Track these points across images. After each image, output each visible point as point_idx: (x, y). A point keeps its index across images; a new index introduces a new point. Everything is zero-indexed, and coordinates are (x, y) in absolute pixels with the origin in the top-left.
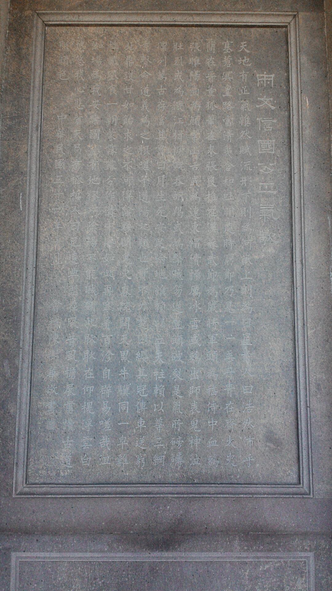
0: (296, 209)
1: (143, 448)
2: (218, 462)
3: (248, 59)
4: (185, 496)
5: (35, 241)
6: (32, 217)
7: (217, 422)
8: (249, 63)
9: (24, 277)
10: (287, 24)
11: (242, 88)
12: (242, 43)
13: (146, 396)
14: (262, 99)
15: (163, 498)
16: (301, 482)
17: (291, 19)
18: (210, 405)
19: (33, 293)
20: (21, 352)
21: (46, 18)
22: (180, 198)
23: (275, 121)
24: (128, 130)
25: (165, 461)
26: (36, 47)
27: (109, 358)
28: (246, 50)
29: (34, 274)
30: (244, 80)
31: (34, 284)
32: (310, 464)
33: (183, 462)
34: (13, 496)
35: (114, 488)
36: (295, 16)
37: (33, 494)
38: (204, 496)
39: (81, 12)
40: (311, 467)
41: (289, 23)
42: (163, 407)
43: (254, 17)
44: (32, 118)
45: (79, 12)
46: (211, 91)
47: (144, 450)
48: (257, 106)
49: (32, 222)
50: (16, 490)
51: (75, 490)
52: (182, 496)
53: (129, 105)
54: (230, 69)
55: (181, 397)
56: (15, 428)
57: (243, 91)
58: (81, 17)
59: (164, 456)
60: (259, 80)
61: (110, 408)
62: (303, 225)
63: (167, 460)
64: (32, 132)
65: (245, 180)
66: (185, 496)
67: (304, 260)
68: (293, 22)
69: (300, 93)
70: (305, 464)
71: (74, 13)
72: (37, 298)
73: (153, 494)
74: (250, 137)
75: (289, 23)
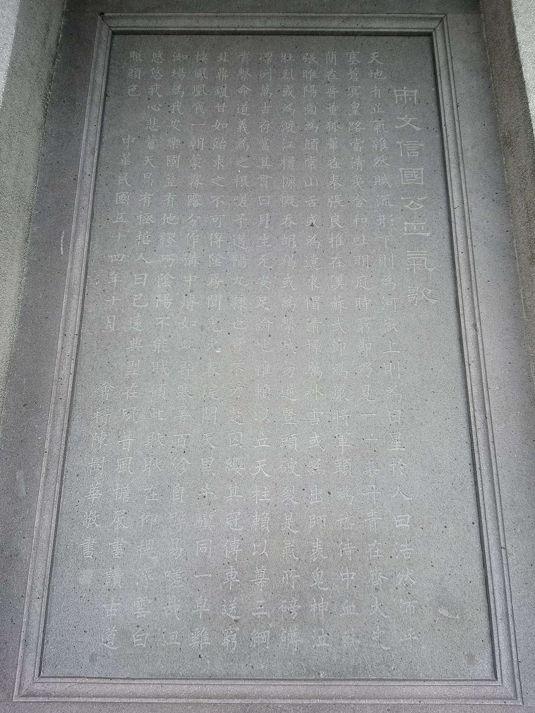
0: (461, 255)
1: (234, 618)
2: (359, 642)
3: (382, 72)
5: (81, 297)
6: (77, 264)
7: (354, 574)
11: (374, 106)
12: (374, 54)
16: (499, 676)
17: (437, 24)
18: (343, 546)
19: (72, 371)
20: (45, 459)
21: (113, 23)
22: (291, 243)
24: (219, 156)
25: (271, 639)
26: (98, 54)
27: (184, 470)
29: (75, 344)
30: (377, 95)
31: (74, 357)
32: (513, 645)
33: (301, 641)
34: (15, 700)
36: (441, 20)
40: (514, 649)
41: (434, 29)
42: (268, 549)
45: (156, 14)
47: (236, 621)
49: (76, 271)
50: (20, 687)
52: (300, 702)
53: (221, 126)
54: (357, 84)
56: (26, 581)
57: (376, 109)
58: (159, 22)
59: (269, 632)
60: (397, 96)
61: (182, 549)
62: (473, 275)
63: (274, 637)
64: (85, 154)
67: (478, 324)
68: (438, 28)
69: (455, 107)
70: (503, 646)
71: (151, 16)
72: (78, 377)
75: (434, 29)
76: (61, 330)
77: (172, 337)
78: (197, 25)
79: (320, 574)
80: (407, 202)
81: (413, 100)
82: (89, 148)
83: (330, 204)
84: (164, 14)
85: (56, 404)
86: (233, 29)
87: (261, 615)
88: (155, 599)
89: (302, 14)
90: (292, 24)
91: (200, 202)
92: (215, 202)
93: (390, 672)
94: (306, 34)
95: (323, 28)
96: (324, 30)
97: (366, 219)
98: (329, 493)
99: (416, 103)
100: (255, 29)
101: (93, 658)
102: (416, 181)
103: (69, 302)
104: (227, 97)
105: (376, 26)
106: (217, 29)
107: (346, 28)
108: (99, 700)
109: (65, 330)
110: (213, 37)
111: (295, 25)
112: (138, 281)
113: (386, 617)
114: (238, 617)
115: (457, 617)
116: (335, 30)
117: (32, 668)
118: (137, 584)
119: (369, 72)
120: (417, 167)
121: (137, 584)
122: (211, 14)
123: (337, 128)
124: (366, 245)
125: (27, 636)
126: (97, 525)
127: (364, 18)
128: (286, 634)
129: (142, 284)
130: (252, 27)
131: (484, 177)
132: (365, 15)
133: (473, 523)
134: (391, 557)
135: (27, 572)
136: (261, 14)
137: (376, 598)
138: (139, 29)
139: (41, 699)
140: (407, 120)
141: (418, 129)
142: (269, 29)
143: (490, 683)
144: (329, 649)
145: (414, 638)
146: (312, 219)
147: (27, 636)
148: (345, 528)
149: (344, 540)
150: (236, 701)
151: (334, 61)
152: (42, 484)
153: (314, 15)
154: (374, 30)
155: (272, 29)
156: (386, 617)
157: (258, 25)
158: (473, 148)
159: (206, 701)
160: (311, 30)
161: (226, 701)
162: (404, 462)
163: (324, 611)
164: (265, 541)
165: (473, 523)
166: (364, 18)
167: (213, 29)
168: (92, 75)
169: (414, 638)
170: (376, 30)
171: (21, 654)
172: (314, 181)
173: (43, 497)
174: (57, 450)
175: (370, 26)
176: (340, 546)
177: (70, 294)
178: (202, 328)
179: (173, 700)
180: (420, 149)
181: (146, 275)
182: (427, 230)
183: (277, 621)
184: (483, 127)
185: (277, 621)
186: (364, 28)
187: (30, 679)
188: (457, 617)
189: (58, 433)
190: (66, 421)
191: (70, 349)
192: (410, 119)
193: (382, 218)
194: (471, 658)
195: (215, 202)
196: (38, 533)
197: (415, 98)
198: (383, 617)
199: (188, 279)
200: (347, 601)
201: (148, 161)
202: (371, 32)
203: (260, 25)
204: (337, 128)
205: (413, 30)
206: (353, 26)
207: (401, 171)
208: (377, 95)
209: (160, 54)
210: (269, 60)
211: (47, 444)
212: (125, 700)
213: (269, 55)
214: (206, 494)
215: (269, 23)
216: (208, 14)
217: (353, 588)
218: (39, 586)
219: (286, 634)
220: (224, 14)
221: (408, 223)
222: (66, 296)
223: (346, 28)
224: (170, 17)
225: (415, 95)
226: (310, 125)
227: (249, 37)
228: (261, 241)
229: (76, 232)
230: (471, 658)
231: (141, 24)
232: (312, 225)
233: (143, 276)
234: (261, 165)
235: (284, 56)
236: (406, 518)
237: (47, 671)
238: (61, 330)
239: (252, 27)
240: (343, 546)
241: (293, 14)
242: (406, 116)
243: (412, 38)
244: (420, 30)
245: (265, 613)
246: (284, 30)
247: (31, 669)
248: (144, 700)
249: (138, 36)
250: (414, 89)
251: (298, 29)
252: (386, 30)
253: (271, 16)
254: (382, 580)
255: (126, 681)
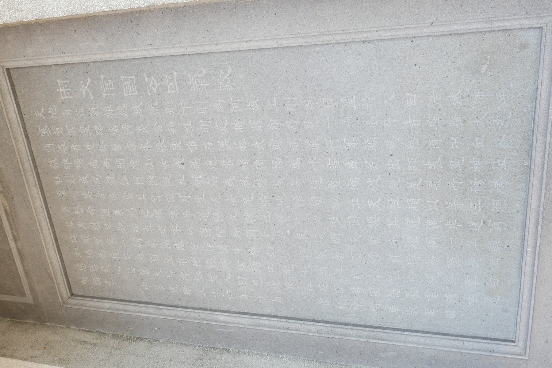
1: (482, 223)
2: (504, 135)
4: (544, 182)
8: (53, 108)
9: (296, 332)
10: (5, 70)
13: (419, 219)
14: (84, 92)
15: (544, 209)
18: (431, 146)
20: (371, 341)
22: (199, 179)
23: (102, 77)
26: (90, 307)
28: (42, 112)
30: (70, 113)
31: (303, 322)
35: (528, 259)
37: (526, 339)
38: (546, 158)
39: (51, 269)
41: (3, 67)
43: (8, 107)
44: (151, 314)
45: (52, 271)
46: (89, 147)
47: (484, 222)
48: (92, 98)
51: (525, 298)
53: (122, 227)
55: (421, 180)
56: (451, 351)
57: (81, 113)
59: (493, 200)
61: (433, 257)
65: (168, 109)
66: (544, 182)
71: (54, 274)
73: (538, 219)
74: (124, 105)
75: (3, 67)
76: (285, 331)
77: (281, 262)
78: (51, 244)
79: (452, 164)
80: (151, 91)
81: (66, 84)
82: (157, 312)
83: (164, 151)
84: (50, 266)
85: (335, 334)
86: (47, 219)
87: (481, 205)
88: (467, 273)
89: (23, 174)
90: (32, 179)
91: (180, 242)
92: (178, 232)
93: (529, 113)
94: (36, 167)
95: (28, 156)
96: (29, 155)
97: (170, 123)
98: (391, 155)
99: (68, 81)
100: (43, 204)
101: (505, 311)
102: (133, 83)
103: (265, 326)
104: (99, 222)
105: (15, 116)
106: (51, 230)
107: (23, 137)
108: (531, 312)
109: (285, 329)
110: (57, 232)
111: (32, 177)
112: (244, 282)
113: (486, 115)
114: (482, 221)
115: (489, 57)
116: (27, 146)
117: (509, 347)
118: (456, 284)
119: (52, 119)
120: (121, 81)
121: (456, 284)
122: (41, 236)
123: (103, 144)
124: (192, 124)
125: (487, 351)
126: (416, 308)
127: (11, 126)
128: (496, 188)
129: (246, 280)
130: (42, 207)
131: (120, 33)
132: (9, 126)
133: (412, 41)
134: (440, 110)
135: (446, 351)
136: (31, 203)
137: (471, 121)
138: (65, 280)
139: (528, 344)
140: (84, 89)
141: (89, 80)
142: (40, 195)
143: (544, 33)
144: (508, 158)
145: (504, 92)
146: (178, 163)
147: (487, 351)
148: (418, 144)
149: (427, 145)
150: (540, 229)
151: (51, 146)
152: (388, 343)
153: (20, 164)
154: (18, 116)
155: (40, 193)
156: (486, 115)
157: (39, 202)
158: (97, 42)
159: (538, 248)
160: (32, 164)
161: (539, 235)
162: (364, 98)
163: (480, 161)
164: (428, 201)
165: (412, 41)
166: (11, 126)
167: (51, 233)
168: (106, 310)
169: (504, 92)
170: (18, 115)
171: (499, 355)
172: (149, 162)
173: (397, 341)
174: (366, 332)
175: (16, 120)
176: (431, 149)
177: (260, 325)
178: (273, 243)
179: (536, 268)
180: (106, 79)
181: (239, 277)
182: (171, 74)
183: (486, 195)
184: (77, 32)
185: (486, 195)
186: (19, 124)
187: (516, 348)
188: (489, 57)
189: (354, 332)
190: (346, 327)
191: (297, 325)
192: (83, 86)
193: (168, 111)
194: (523, 46)
195: (178, 232)
196: (421, 344)
197: (64, 82)
198: (486, 117)
199: (237, 251)
200: (473, 144)
201: (158, 274)
202: (20, 118)
203: (39, 201)
204: (103, 144)
205: (9, 85)
206: (20, 133)
207: (127, 95)
208: (70, 113)
209: (78, 265)
210: (63, 193)
211: (362, 340)
212: (533, 297)
213: (60, 193)
214: (394, 241)
215: (35, 195)
216: (42, 238)
217: (463, 139)
218: (456, 343)
219: (496, 188)
220: (39, 227)
221: (169, 90)
222: (261, 328)
223: (23, 137)
224: (51, 263)
225: (62, 82)
226: (106, 164)
227: (49, 206)
228: (201, 201)
229: (217, 321)
230: (523, 46)
231: (60, 279)
232: (183, 164)
233: (240, 279)
234: (143, 200)
235: (57, 183)
236: (409, 97)
237: (510, 337)
238: (285, 331)
239: (42, 207)
240: (431, 146)
241: (25, 180)
242: (81, 89)
243: (15, 83)
244: (7, 78)
245: (480, 202)
246: (37, 183)
247: (509, 348)
248: (534, 286)
249: (70, 279)
250: (57, 83)
251: (34, 173)
252: (15, 107)
253: (31, 195)
254: (457, 117)
255: (521, 293)
